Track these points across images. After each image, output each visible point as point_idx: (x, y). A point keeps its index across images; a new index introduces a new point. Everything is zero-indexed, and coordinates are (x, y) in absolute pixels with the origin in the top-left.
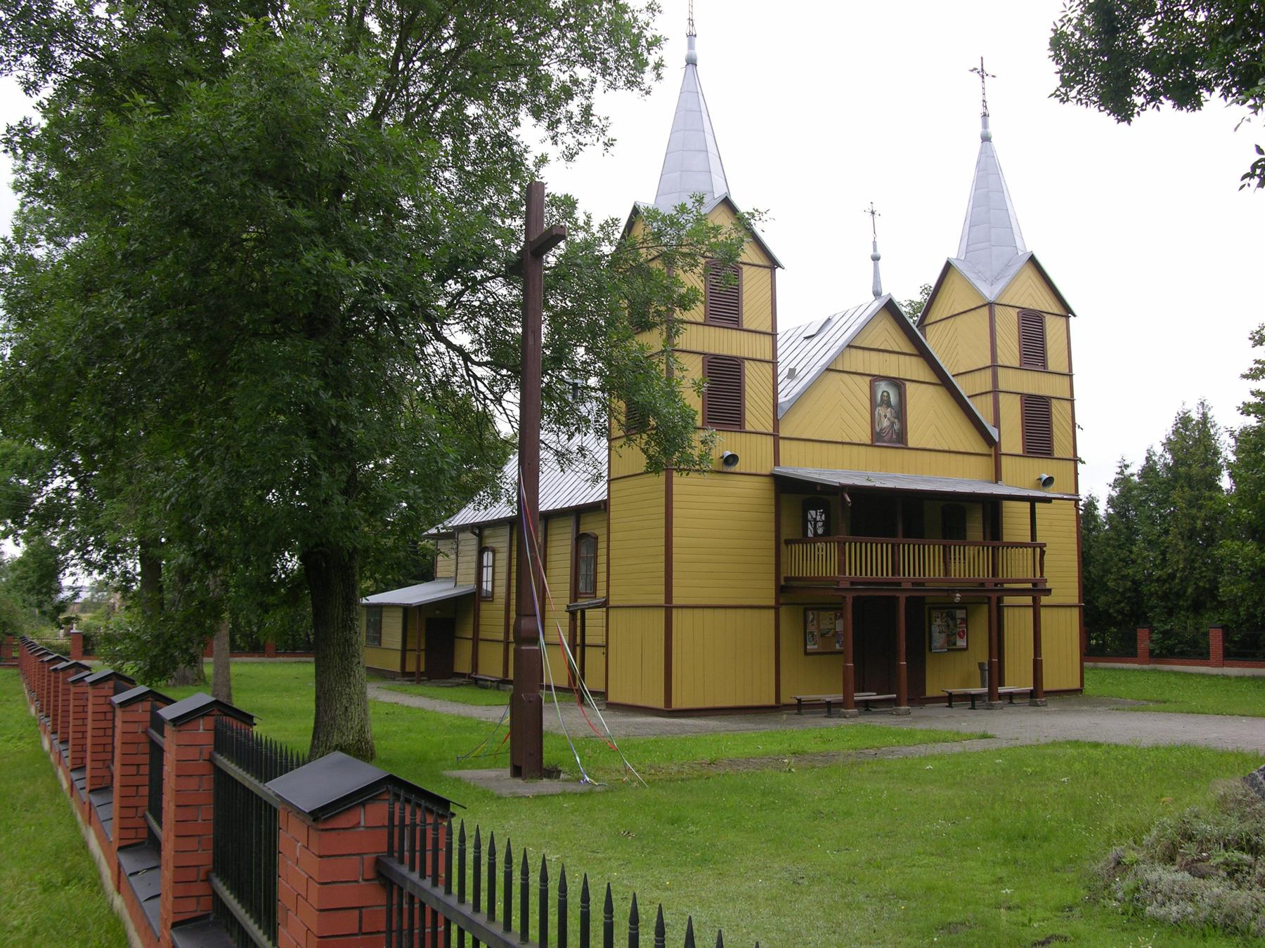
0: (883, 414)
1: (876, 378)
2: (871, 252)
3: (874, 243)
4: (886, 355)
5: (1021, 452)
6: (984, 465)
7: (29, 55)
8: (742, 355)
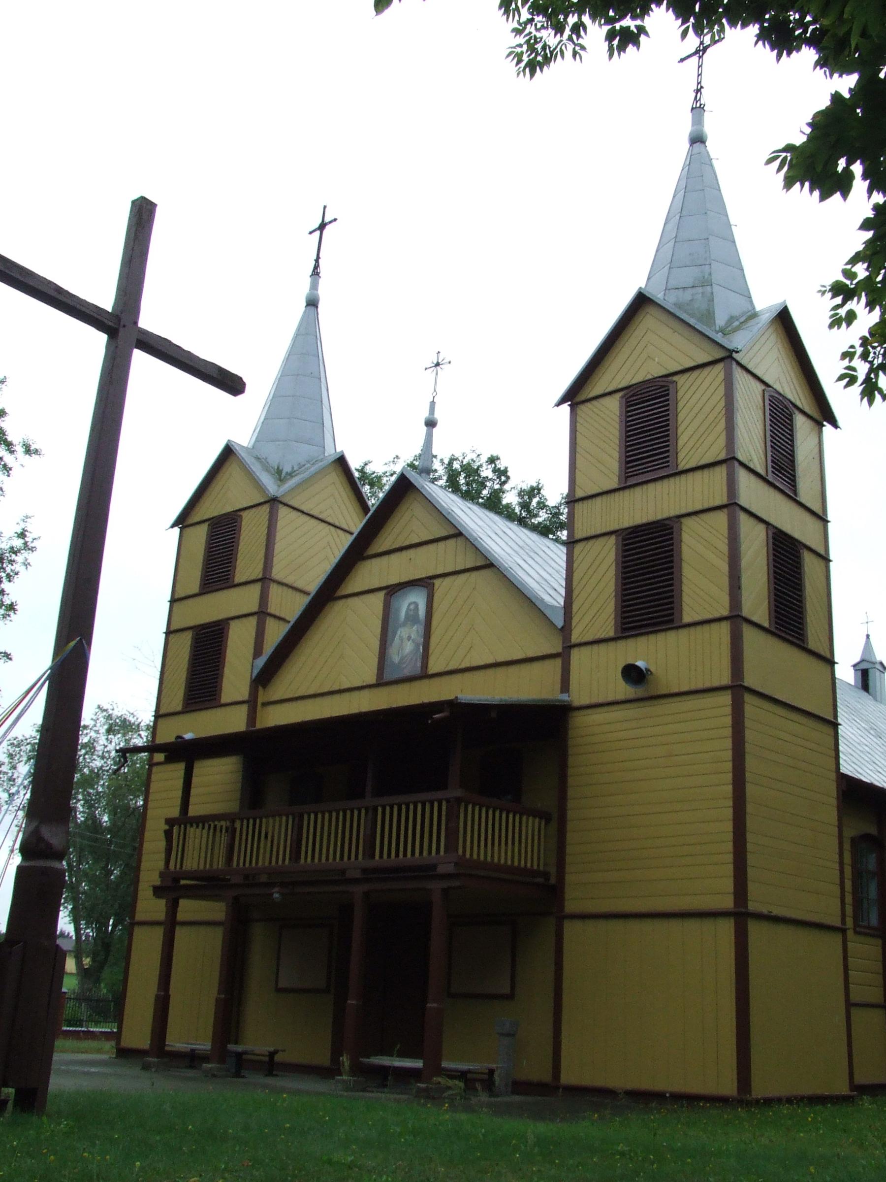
0: (405, 636)
1: (393, 591)
2: (426, 414)
3: (433, 404)
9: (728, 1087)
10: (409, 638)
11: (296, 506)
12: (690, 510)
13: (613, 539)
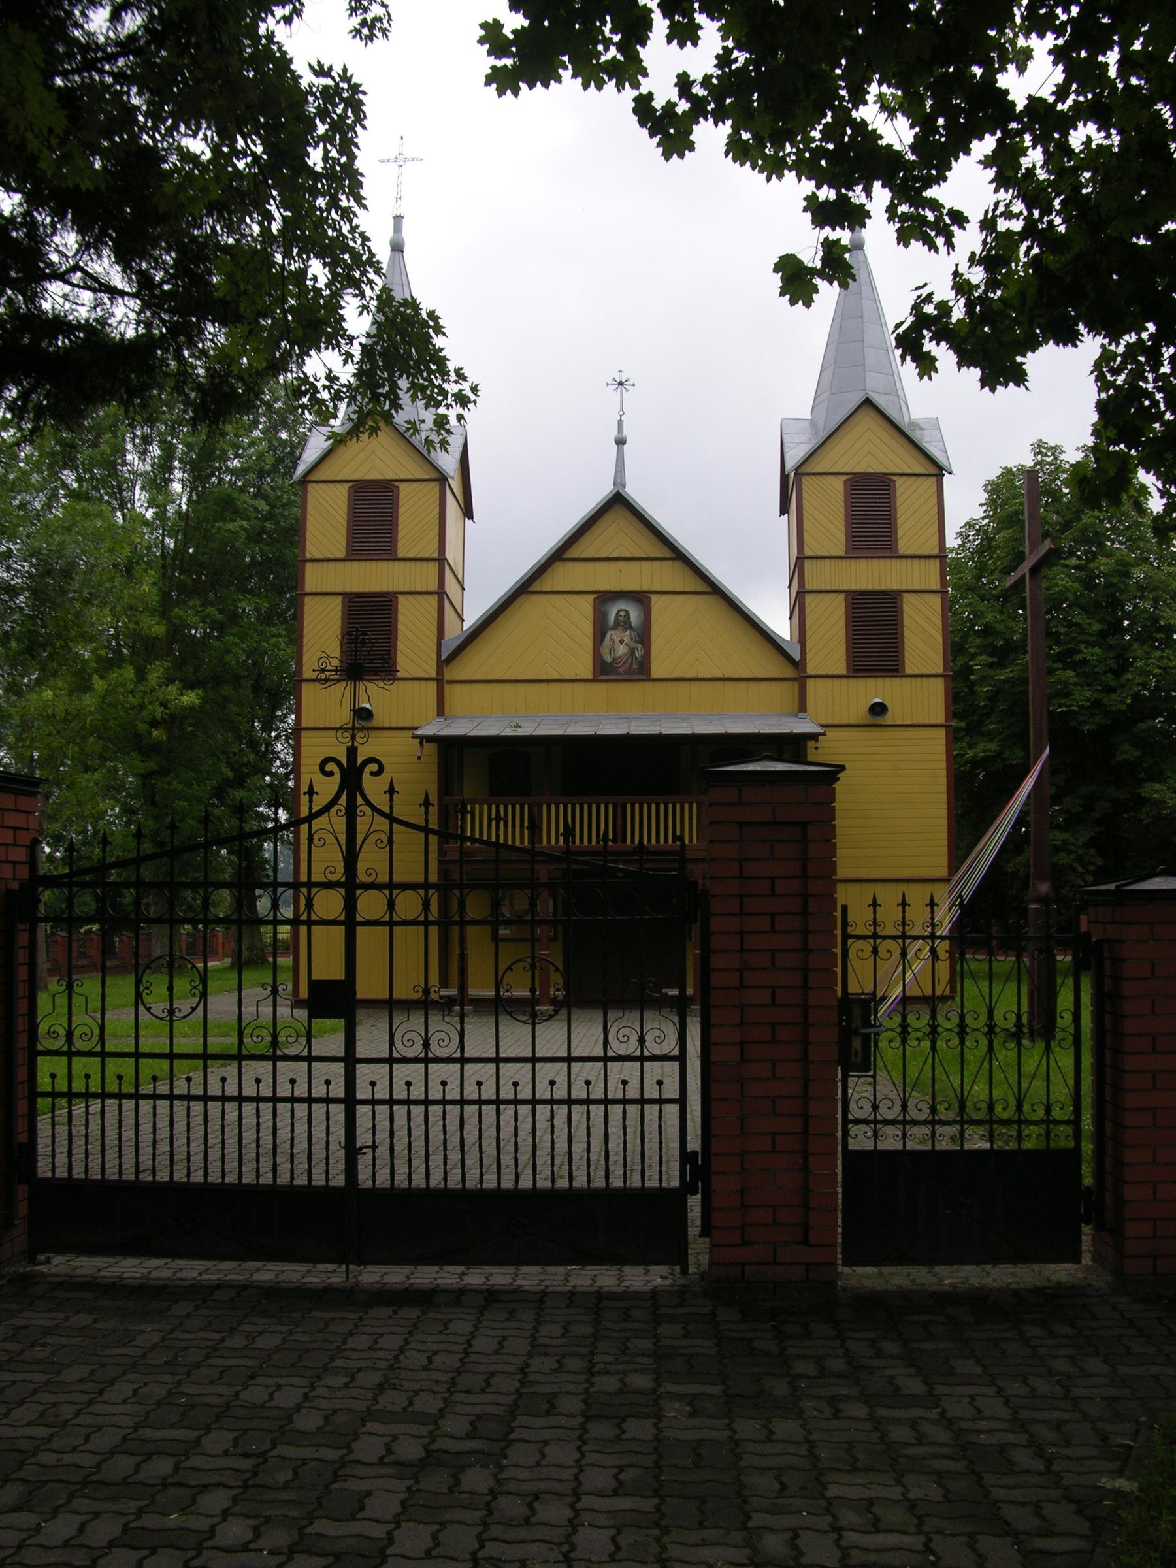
0: (617, 639)
1: (604, 598)
2: (614, 433)
3: (620, 422)
4: (622, 564)
5: (844, 672)
6: (788, 691)
7: (1047, 93)
8: (396, 589)
9: (676, 1064)
10: (622, 642)
11: (331, 478)
12: (407, 589)
13: (340, 598)
